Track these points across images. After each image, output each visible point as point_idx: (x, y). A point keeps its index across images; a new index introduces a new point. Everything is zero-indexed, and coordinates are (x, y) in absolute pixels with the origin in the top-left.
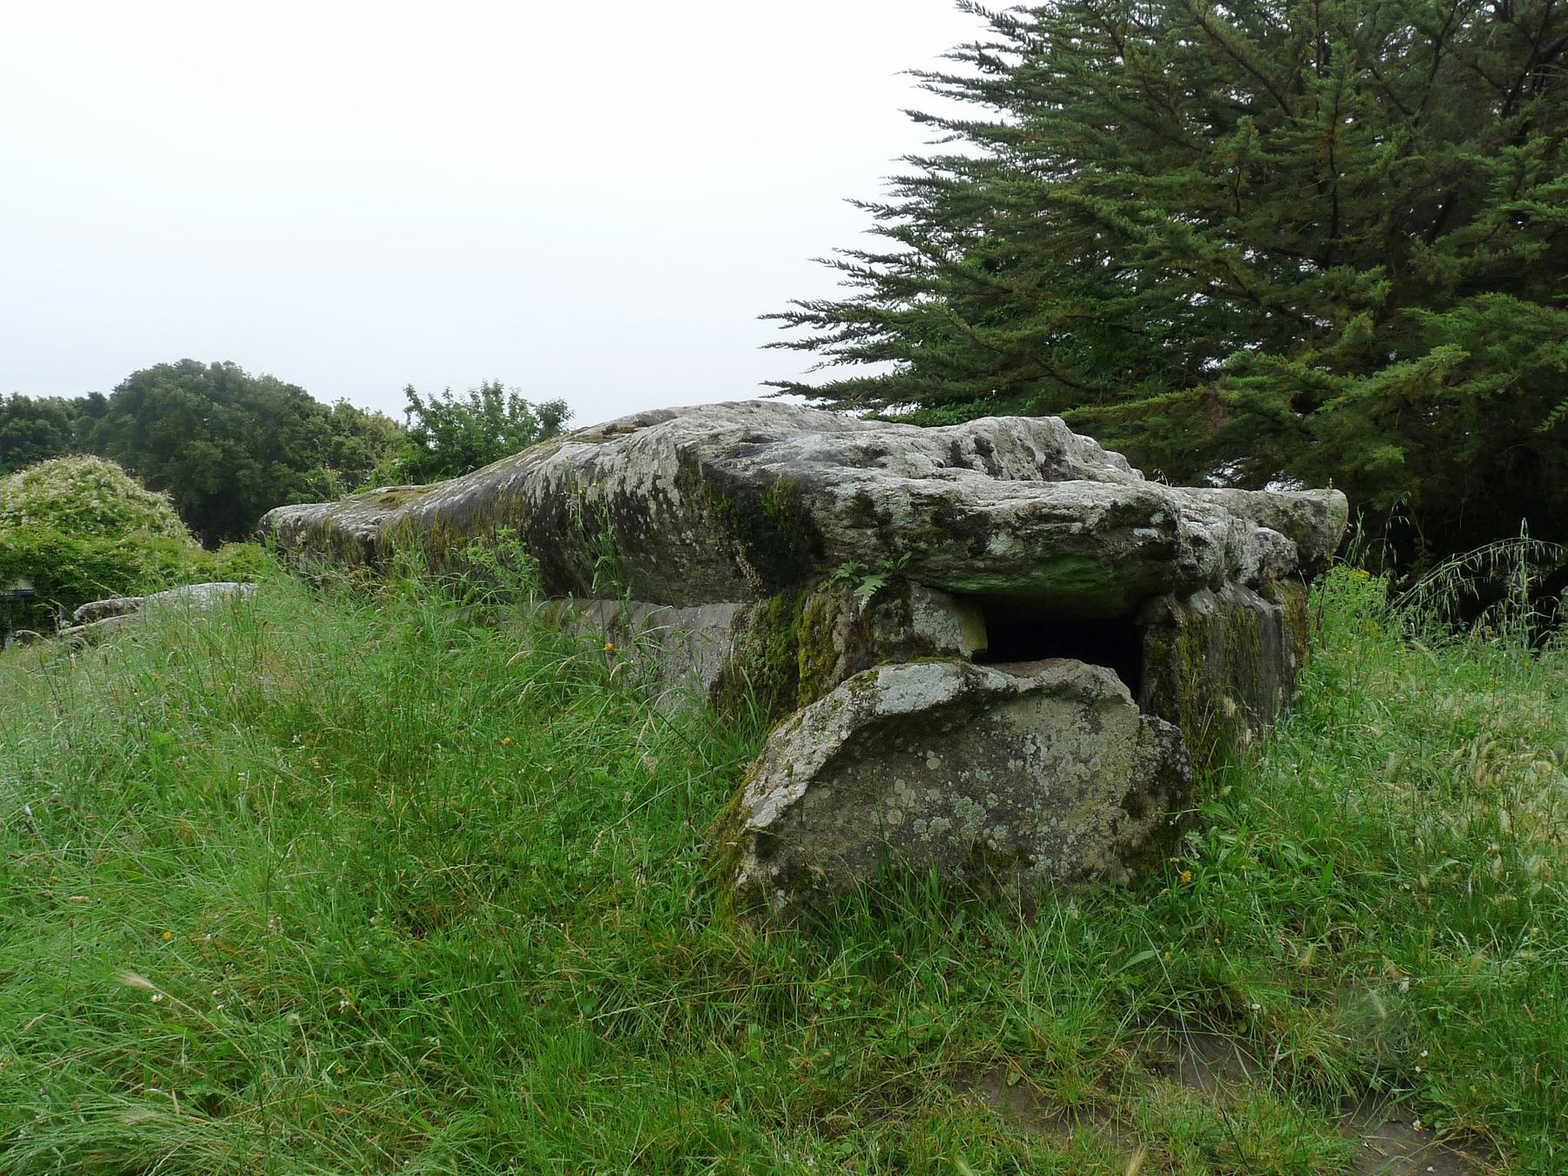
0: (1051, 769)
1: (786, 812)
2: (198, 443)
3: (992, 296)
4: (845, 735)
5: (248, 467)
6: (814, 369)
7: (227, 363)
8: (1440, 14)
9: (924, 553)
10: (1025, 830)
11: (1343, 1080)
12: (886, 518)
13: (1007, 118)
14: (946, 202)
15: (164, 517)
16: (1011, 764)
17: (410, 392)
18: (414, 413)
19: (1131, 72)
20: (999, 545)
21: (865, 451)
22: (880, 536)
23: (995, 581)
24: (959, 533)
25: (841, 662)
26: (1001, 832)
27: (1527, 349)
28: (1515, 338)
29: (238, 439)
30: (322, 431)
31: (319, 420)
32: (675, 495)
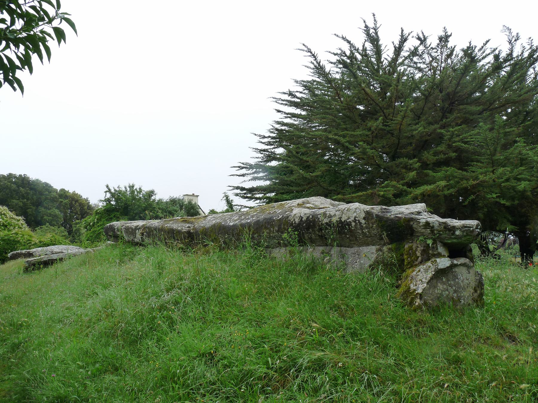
1: (424, 290)
2: (14, 201)
4: (433, 273)
5: (30, 208)
6: (242, 182)
7: (24, 175)
8: (428, 91)
9: (441, 234)
10: (459, 295)
11: (462, 354)
12: (433, 227)
13: (298, 111)
14: (282, 136)
15: (22, 225)
16: (457, 280)
17: (107, 186)
18: (108, 193)
19: (345, 102)
20: (458, 233)
21: (418, 212)
22: (431, 231)
23: (455, 241)
24: (450, 230)
25: (420, 258)
26: (455, 295)
27: (458, 182)
28: (456, 179)
29: (28, 199)
30: (56, 197)
31: (55, 194)
32: (363, 222)
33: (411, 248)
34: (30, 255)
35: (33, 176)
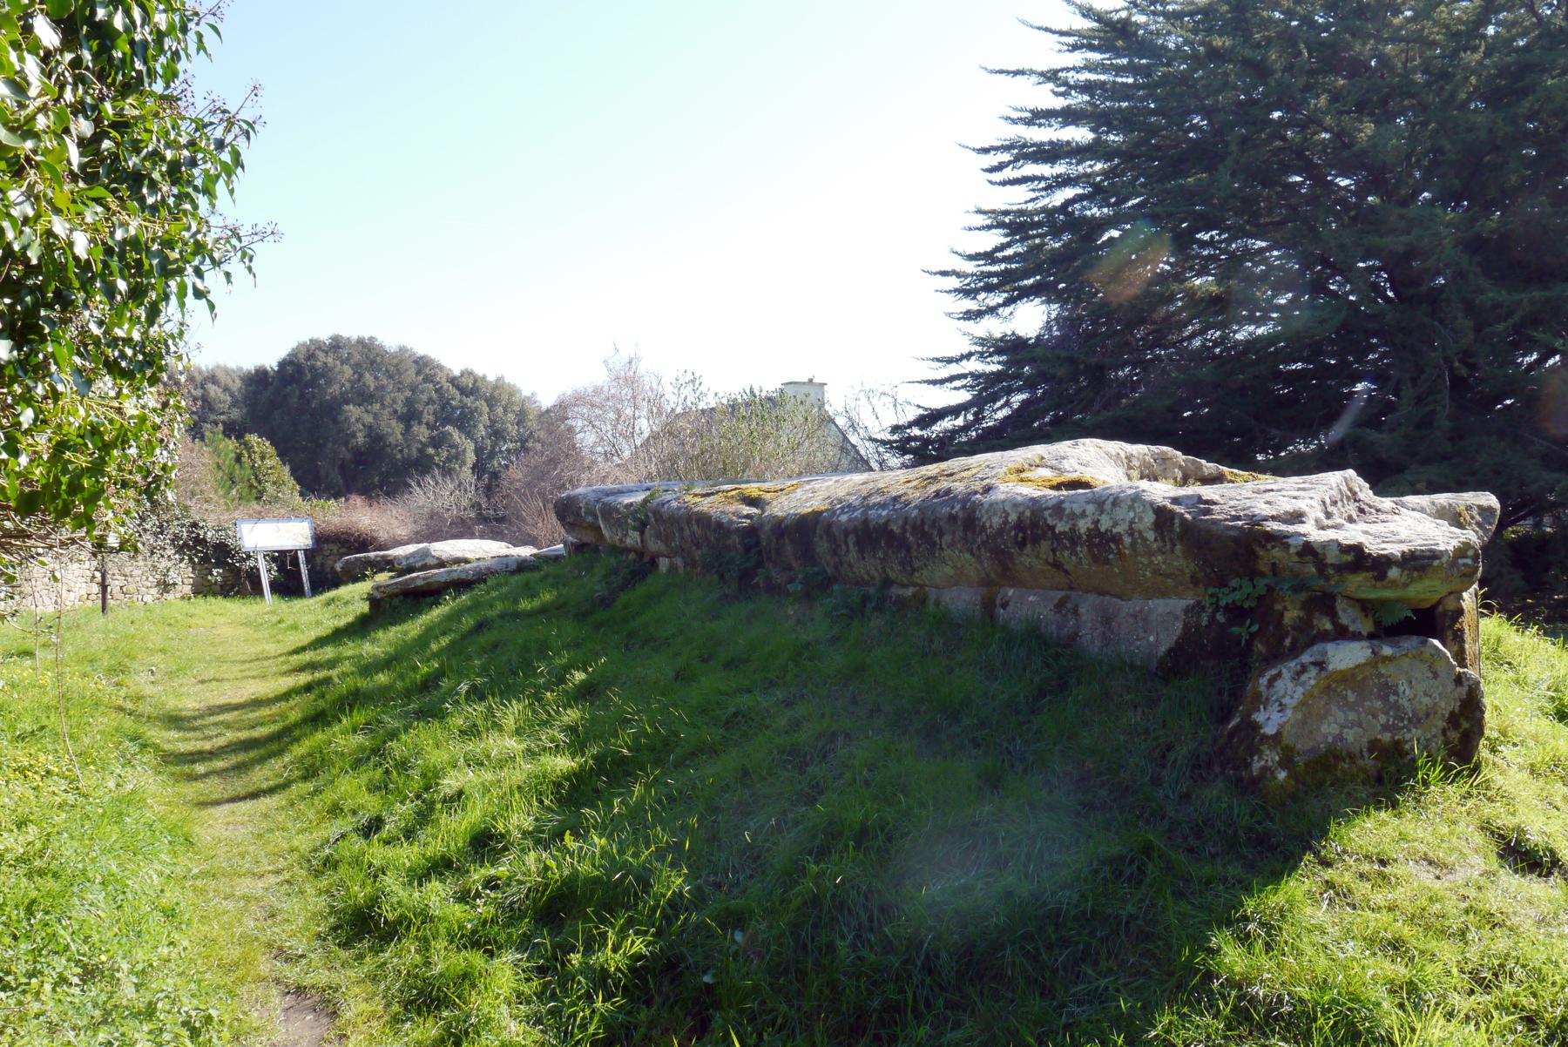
13: (1080, 134)
35: (390, 341)
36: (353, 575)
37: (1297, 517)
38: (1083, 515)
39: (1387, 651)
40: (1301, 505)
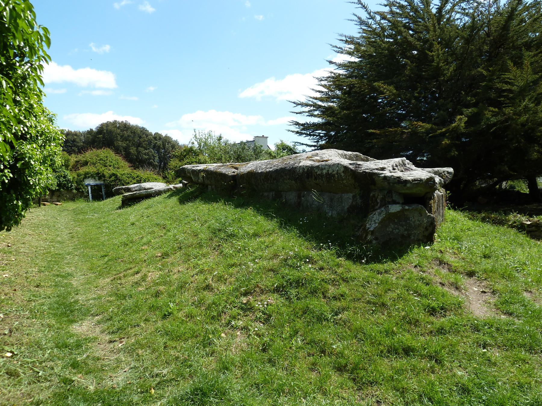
0: (414, 222)
1: (375, 228)
3: (352, 112)
25: (379, 205)
26: (406, 232)
32: (343, 174)
33: (374, 196)
34: (129, 190)
36: (118, 192)
37: (383, 169)
38: (325, 169)
39: (407, 207)
40: (385, 166)
